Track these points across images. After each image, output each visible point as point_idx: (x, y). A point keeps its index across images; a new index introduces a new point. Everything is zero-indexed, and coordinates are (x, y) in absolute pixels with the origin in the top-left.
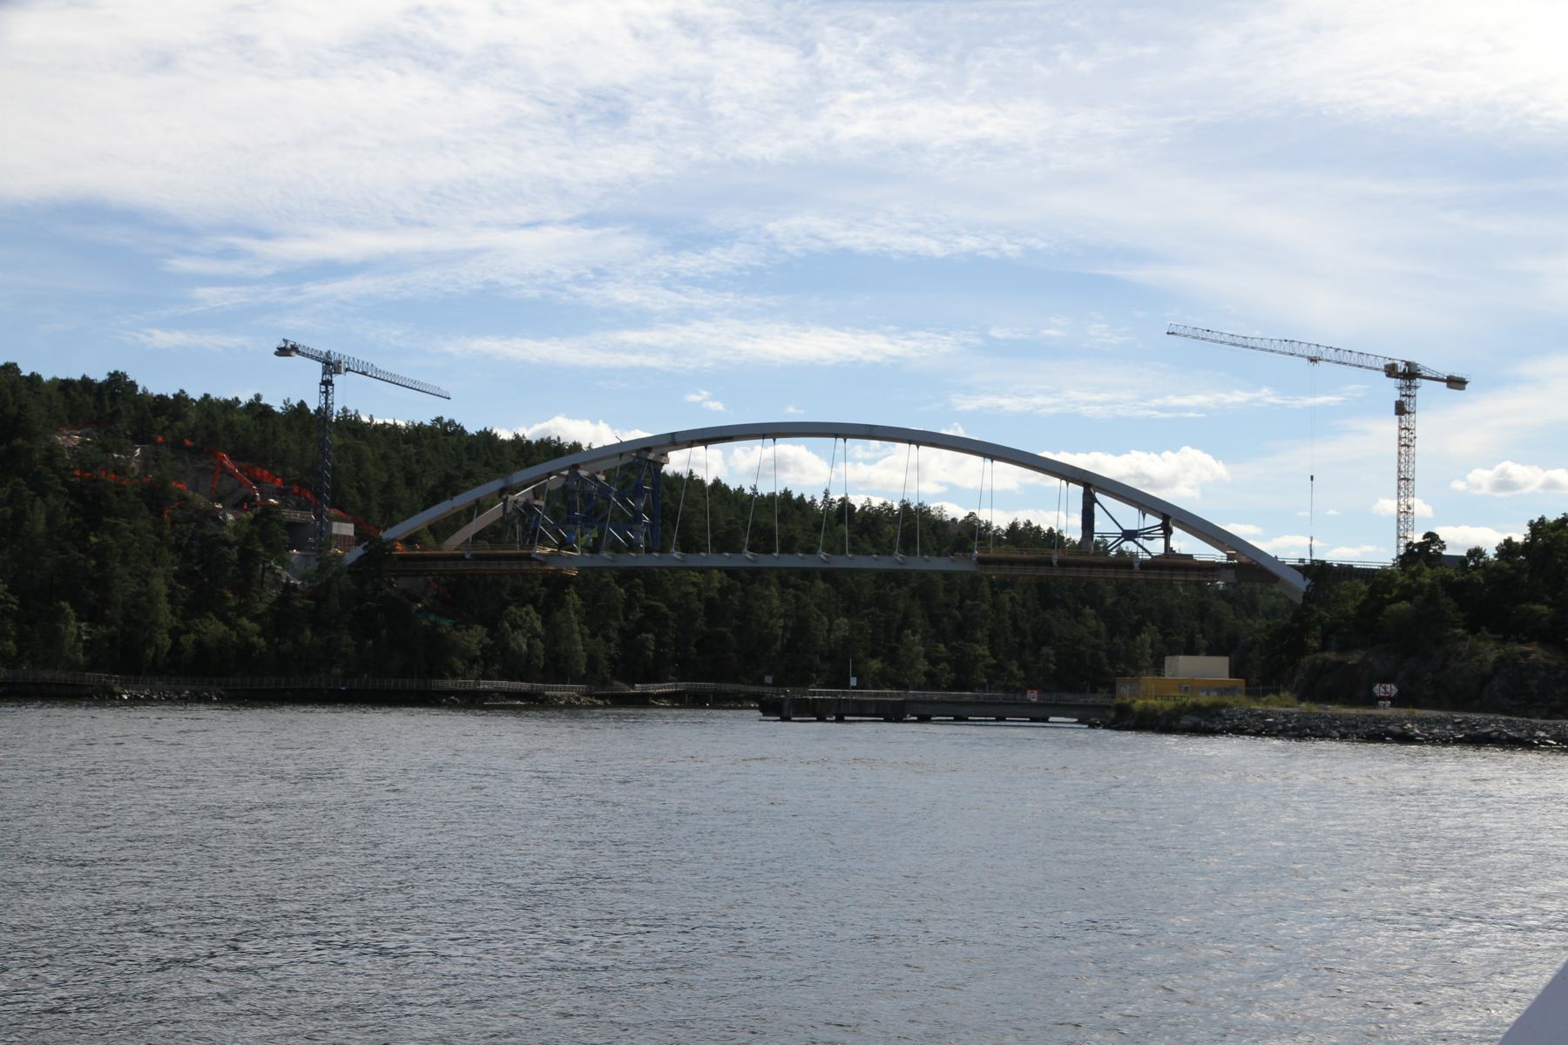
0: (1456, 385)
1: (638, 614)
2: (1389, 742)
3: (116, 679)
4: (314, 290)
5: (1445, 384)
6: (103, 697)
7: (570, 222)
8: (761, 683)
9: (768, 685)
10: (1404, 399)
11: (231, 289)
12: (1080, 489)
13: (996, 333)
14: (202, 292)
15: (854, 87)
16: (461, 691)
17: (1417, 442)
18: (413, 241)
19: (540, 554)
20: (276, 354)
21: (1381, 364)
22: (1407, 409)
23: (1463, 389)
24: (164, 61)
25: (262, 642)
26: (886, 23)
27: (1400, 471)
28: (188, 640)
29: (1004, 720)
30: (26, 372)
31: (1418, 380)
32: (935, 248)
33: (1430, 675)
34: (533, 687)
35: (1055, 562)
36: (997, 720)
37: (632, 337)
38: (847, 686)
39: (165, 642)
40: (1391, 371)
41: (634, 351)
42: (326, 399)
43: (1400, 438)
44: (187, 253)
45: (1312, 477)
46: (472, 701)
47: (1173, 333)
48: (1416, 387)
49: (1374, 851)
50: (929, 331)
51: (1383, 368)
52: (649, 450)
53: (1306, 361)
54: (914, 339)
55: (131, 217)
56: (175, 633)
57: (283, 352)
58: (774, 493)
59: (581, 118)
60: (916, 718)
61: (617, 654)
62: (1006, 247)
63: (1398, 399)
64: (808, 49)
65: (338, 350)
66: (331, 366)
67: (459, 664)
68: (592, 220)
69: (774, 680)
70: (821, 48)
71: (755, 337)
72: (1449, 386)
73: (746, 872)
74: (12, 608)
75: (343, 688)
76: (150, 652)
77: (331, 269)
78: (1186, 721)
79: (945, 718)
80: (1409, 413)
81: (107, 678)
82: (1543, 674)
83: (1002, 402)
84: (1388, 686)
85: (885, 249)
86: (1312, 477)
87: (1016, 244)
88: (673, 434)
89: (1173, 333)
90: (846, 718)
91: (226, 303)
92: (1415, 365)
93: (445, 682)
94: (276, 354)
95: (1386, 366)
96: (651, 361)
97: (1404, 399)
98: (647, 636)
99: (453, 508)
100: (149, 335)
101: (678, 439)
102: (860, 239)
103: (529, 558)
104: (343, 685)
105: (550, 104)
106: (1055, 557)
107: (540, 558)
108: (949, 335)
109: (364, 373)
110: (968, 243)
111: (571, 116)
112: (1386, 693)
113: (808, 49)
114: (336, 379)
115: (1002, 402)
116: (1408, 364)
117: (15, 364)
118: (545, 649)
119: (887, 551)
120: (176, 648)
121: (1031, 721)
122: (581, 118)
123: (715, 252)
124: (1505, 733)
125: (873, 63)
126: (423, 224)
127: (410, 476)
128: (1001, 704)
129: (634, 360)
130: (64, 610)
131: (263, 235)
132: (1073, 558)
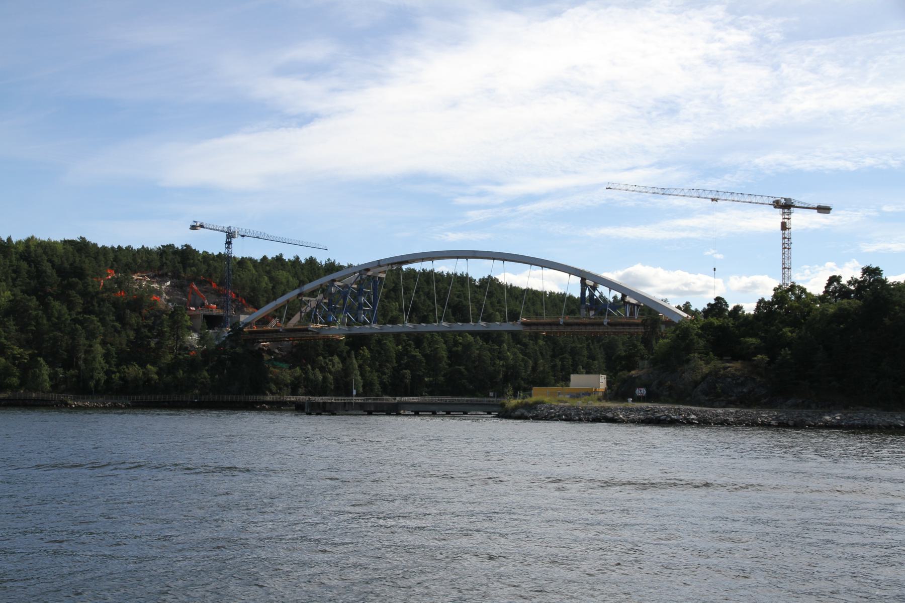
0: (823, 211)
3: (71, 397)
4: (523, 208)
5: (816, 211)
6: (61, 406)
7: (651, 166)
8: (488, 396)
9: (491, 397)
10: (786, 220)
11: (482, 211)
12: (580, 279)
13: (886, 208)
14: (471, 213)
16: (280, 402)
19: (313, 328)
20: (190, 229)
21: (771, 201)
24: (454, 104)
25: (156, 377)
27: (783, 264)
30: (100, 246)
31: (792, 209)
32: (850, 166)
33: (669, 382)
35: (605, 323)
37: (683, 222)
38: (351, 394)
39: (102, 377)
40: (777, 204)
42: (228, 251)
43: (783, 244)
44: (463, 195)
45: (715, 269)
46: (278, 407)
47: (609, 188)
49: (127, 485)
51: (772, 203)
53: (710, 201)
54: (838, 215)
55: (438, 179)
56: (108, 373)
57: (193, 228)
58: (565, 294)
59: (654, 114)
62: (892, 162)
64: (776, 67)
65: (235, 225)
66: (230, 236)
67: (273, 387)
68: (661, 165)
70: (783, 66)
72: (818, 212)
73: (600, 505)
74: (24, 362)
75: (196, 401)
76: (92, 384)
77: (531, 198)
78: (517, 413)
82: (729, 380)
84: (642, 389)
86: (715, 269)
87: (898, 160)
88: (379, 261)
89: (609, 188)
90: (420, 413)
91: (481, 218)
92: (790, 199)
94: (190, 229)
95: (774, 202)
97: (786, 220)
98: (406, 371)
100: (447, 235)
101: (381, 263)
103: (307, 330)
104: (196, 399)
105: (638, 108)
106: (606, 321)
107: (314, 330)
108: (859, 212)
109: (258, 237)
110: (869, 161)
111: (649, 113)
112: (641, 393)
113: (776, 67)
114: (233, 241)
116: (785, 199)
117: (33, 237)
118: (334, 379)
120: (108, 381)
121: (488, 414)
122: (654, 114)
123: (727, 177)
124: (670, 417)
126: (575, 172)
127: (86, 285)
128: (485, 404)
129: (684, 235)
130: (39, 361)
131: (498, 184)
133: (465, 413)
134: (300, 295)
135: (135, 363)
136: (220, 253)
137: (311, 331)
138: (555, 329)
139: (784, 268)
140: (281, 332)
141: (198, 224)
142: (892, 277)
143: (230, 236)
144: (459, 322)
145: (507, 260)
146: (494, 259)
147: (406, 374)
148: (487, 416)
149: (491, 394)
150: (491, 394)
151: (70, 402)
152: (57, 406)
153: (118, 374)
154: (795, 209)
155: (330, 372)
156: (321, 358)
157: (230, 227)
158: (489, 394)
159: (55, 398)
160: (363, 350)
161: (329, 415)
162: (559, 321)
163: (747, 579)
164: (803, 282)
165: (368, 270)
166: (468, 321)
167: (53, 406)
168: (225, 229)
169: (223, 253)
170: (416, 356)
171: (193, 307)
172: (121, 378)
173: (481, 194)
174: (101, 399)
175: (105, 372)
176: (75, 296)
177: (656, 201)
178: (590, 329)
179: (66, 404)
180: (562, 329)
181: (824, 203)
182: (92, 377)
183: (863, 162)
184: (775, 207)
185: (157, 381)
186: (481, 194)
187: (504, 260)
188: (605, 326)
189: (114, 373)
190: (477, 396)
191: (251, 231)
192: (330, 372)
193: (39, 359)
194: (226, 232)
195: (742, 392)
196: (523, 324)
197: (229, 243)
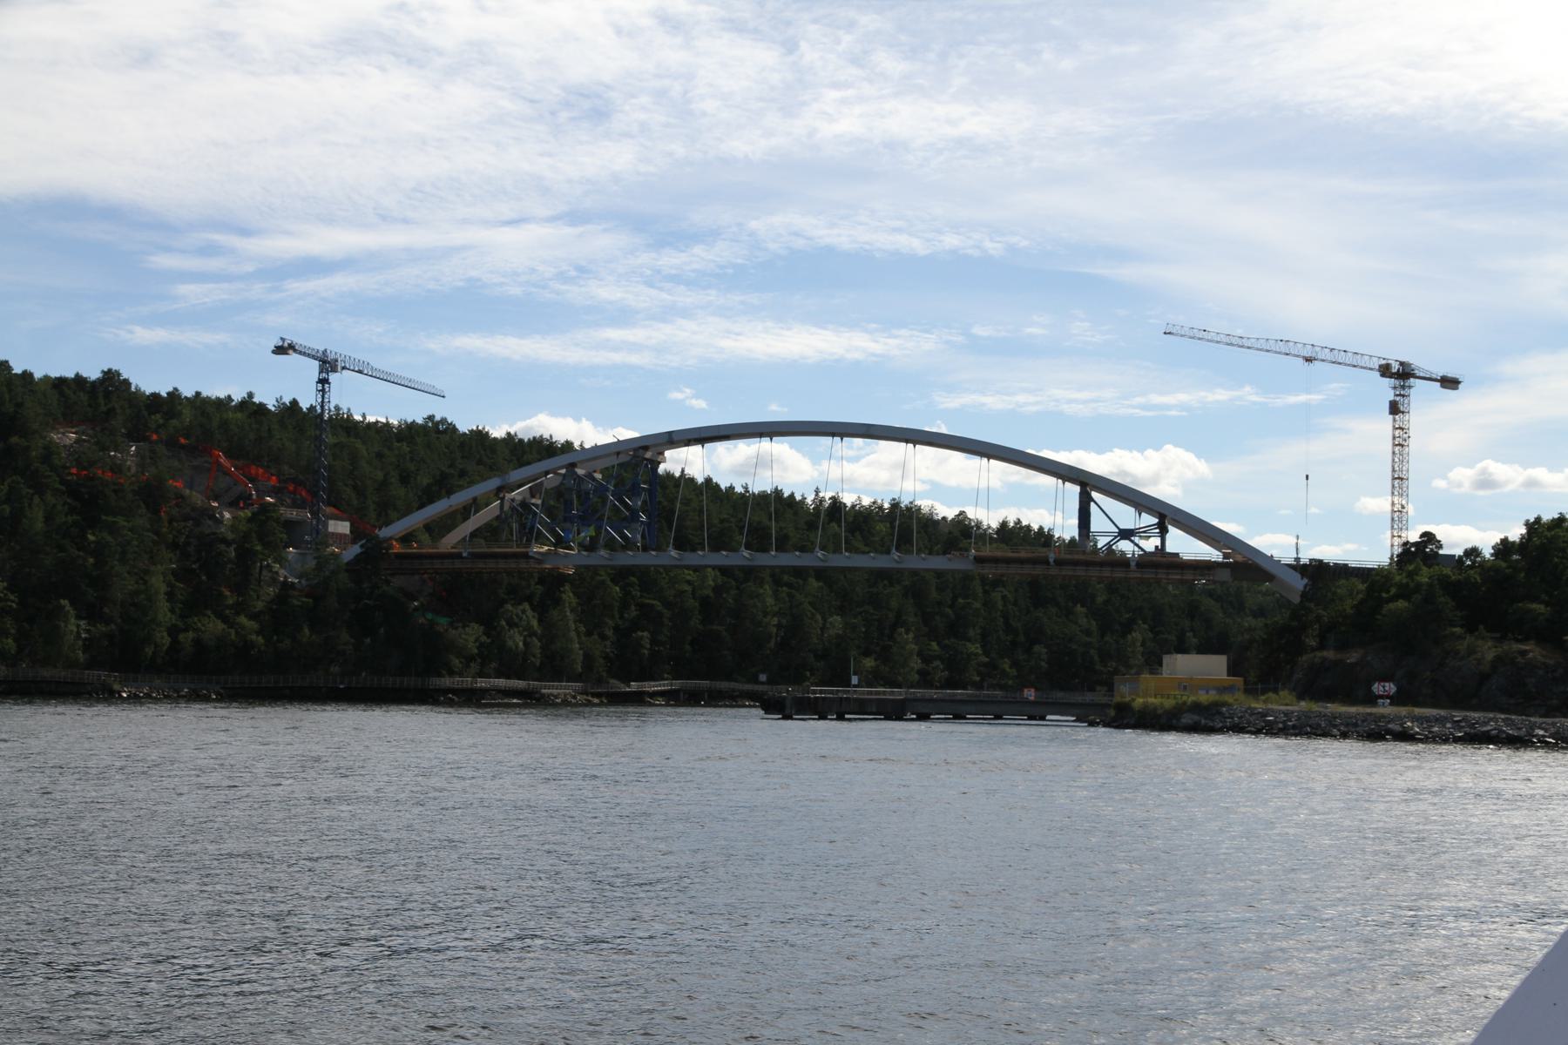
0: (1449, 385)
3: (115, 677)
4: (297, 287)
5: (1439, 384)
9: (763, 683)
10: (1398, 399)
11: (211, 286)
12: (1077, 489)
13: (978, 330)
14: (184, 289)
15: (836, 85)
17: (1412, 442)
18: (394, 238)
20: (274, 352)
21: (1376, 364)
23: (1456, 388)
25: (260, 640)
27: (1394, 471)
28: (187, 638)
35: (1051, 560)
40: (1385, 371)
43: (1394, 438)
44: (168, 250)
45: (1307, 477)
47: (1169, 333)
48: (1410, 387)
50: (912, 330)
52: (646, 448)
54: (896, 337)
56: (173, 631)
57: (280, 350)
59: (564, 115)
61: (613, 652)
62: (989, 245)
63: (1392, 398)
64: (790, 47)
65: (335, 349)
66: (328, 365)
67: (456, 662)
68: (575, 217)
70: (803, 45)
72: (1443, 386)
74: (11, 606)
75: (342, 686)
76: (149, 651)
78: (1187, 719)
82: (1541, 672)
84: (1387, 684)
85: (867, 247)
86: (1307, 477)
88: (670, 433)
89: (1169, 333)
91: (207, 300)
93: (443, 679)
94: (274, 352)
95: (1380, 366)
96: (634, 359)
97: (1398, 399)
100: (131, 332)
101: (675, 438)
102: (843, 237)
103: (526, 556)
104: (341, 683)
105: (532, 101)
107: (537, 556)
108: (932, 334)
110: (951, 241)
111: (553, 113)
112: (1385, 691)
113: (790, 47)
114: (333, 377)
116: (1402, 364)
120: (175, 645)
123: (698, 250)
125: (855, 61)
126: (406, 221)
129: (617, 357)
131: (245, 232)
132: (1069, 557)
133: (998, 717)
135: (209, 612)
136: (294, 403)
137: (533, 558)
138: (1039, 570)
140: (465, 558)
144: (796, 550)
147: (642, 638)
148: (1028, 722)
154: (1417, 380)
158: (850, 680)
161: (818, 719)
162: (1047, 556)
163: (980, 1014)
164: (1155, 480)
165: (646, 448)
166: (765, 550)
169: (304, 405)
170: (653, 605)
171: (270, 503)
173: (209, 250)
174: (157, 682)
177: (564, 287)
178: (1027, 570)
180: (1054, 571)
181: (1451, 374)
183: (940, 241)
184: (1383, 375)
185: (263, 648)
186: (209, 250)
190: (736, 681)
191: (352, 359)
193: (62, 601)
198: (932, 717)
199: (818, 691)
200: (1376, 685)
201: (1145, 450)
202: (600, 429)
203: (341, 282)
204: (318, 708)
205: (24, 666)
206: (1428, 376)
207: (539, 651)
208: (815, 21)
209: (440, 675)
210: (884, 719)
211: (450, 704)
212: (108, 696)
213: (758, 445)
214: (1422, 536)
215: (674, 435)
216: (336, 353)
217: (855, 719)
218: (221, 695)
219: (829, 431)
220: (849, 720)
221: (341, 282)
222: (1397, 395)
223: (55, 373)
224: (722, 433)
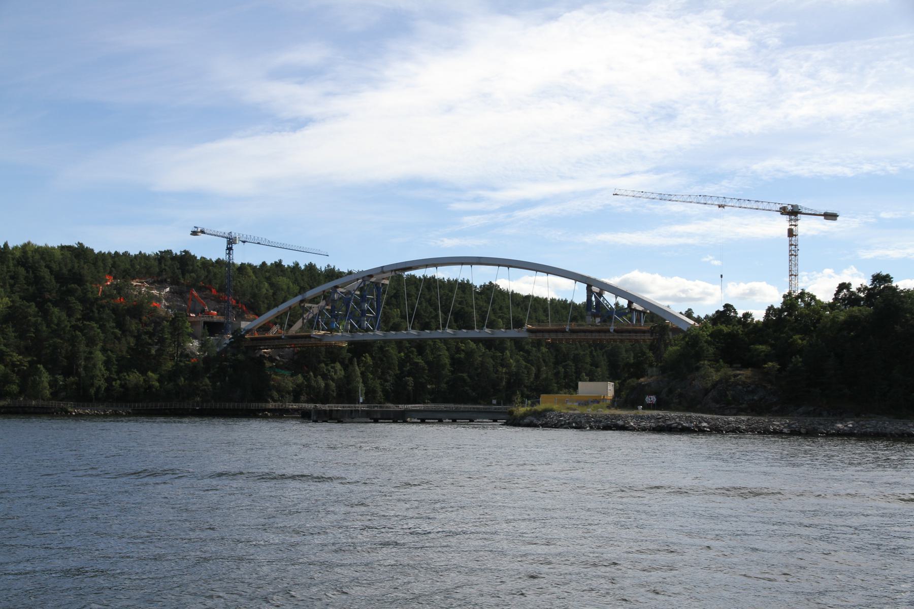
0: (829, 217)
1: (408, 368)
2: (614, 430)
4: (519, 214)
5: (823, 217)
8: (491, 403)
9: (494, 405)
10: (793, 227)
13: (883, 215)
15: (800, 90)
17: (799, 253)
18: (567, 187)
20: (191, 234)
21: (778, 207)
22: (794, 233)
23: (836, 220)
25: (157, 384)
26: (818, 54)
28: (116, 384)
29: (473, 421)
32: (848, 172)
34: (316, 406)
35: (612, 331)
36: (470, 422)
38: (491, 403)
39: (103, 384)
40: (784, 211)
41: (681, 236)
42: (229, 256)
43: (790, 251)
44: (459, 200)
45: (722, 276)
46: (280, 414)
48: (797, 220)
50: (845, 217)
52: (371, 276)
55: (433, 185)
56: (109, 380)
57: (194, 233)
60: (419, 421)
61: (391, 389)
62: (889, 168)
63: (788, 227)
64: (774, 73)
65: (236, 232)
66: (231, 242)
68: (658, 170)
69: (497, 402)
70: (781, 71)
71: (746, 225)
75: (197, 408)
76: (92, 391)
77: (527, 204)
78: (526, 421)
79: (432, 421)
80: (795, 235)
81: (65, 404)
82: (740, 387)
83: (888, 253)
85: (819, 174)
86: (722, 276)
87: (896, 166)
88: (382, 267)
90: (426, 421)
92: (797, 206)
93: (267, 404)
94: (191, 234)
95: (781, 208)
96: (690, 241)
97: (793, 227)
99: (279, 312)
100: (442, 241)
101: (385, 270)
102: (803, 170)
103: (309, 337)
105: (635, 113)
110: (867, 168)
111: (646, 118)
112: (651, 401)
113: (774, 73)
114: (234, 247)
115: (888, 253)
116: (792, 206)
117: (29, 243)
119: (470, 327)
123: (725, 183)
124: (682, 425)
125: (811, 76)
126: (572, 178)
129: (681, 241)
130: (39, 368)
131: (494, 189)
132: (577, 328)
134: (302, 301)
135: (135, 371)
139: (791, 275)
140: (283, 339)
141: (199, 230)
142: (903, 283)
143: (231, 242)
145: (512, 267)
146: (499, 265)
147: (408, 380)
149: (494, 402)
150: (494, 402)
151: (70, 410)
152: (57, 413)
153: (118, 382)
155: (333, 380)
156: (323, 365)
157: (231, 233)
159: (55, 406)
160: (365, 357)
167: (53, 413)
168: (226, 235)
171: (192, 313)
172: (122, 386)
173: (477, 199)
175: (105, 379)
176: (74, 303)
179: (67, 412)
181: (830, 210)
182: (92, 385)
185: (158, 388)
186: (477, 199)
187: (509, 266)
188: (611, 333)
189: (115, 380)
190: (480, 404)
191: (253, 237)
192: (333, 380)
193: (39, 366)
194: (227, 238)
195: (753, 400)
196: (529, 331)
197: (230, 249)
198: (426, 421)
199: (254, 406)
200: (647, 398)
201: (823, 270)
202: (664, 278)
203: (541, 210)
204: (177, 420)
205: (21, 399)
206: (813, 213)
207: (335, 389)
208: (788, 58)
209: (267, 402)
210: (393, 422)
211: (265, 417)
212: (64, 414)
213: (534, 277)
214: (724, 307)
215: (384, 268)
216: (262, 238)
217: (385, 422)
218: (129, 413)
219: (460, 262)
220: (429, 423)
221: (541, 210)
222: (791, 225)
223: (105, 250)
224: (408, 266)
